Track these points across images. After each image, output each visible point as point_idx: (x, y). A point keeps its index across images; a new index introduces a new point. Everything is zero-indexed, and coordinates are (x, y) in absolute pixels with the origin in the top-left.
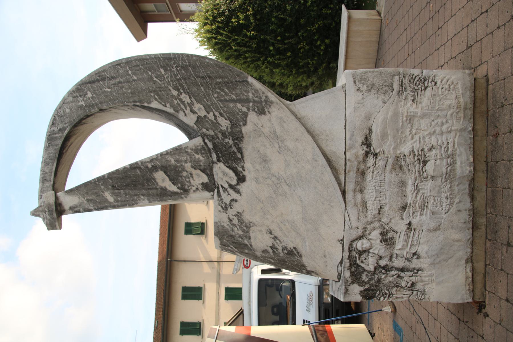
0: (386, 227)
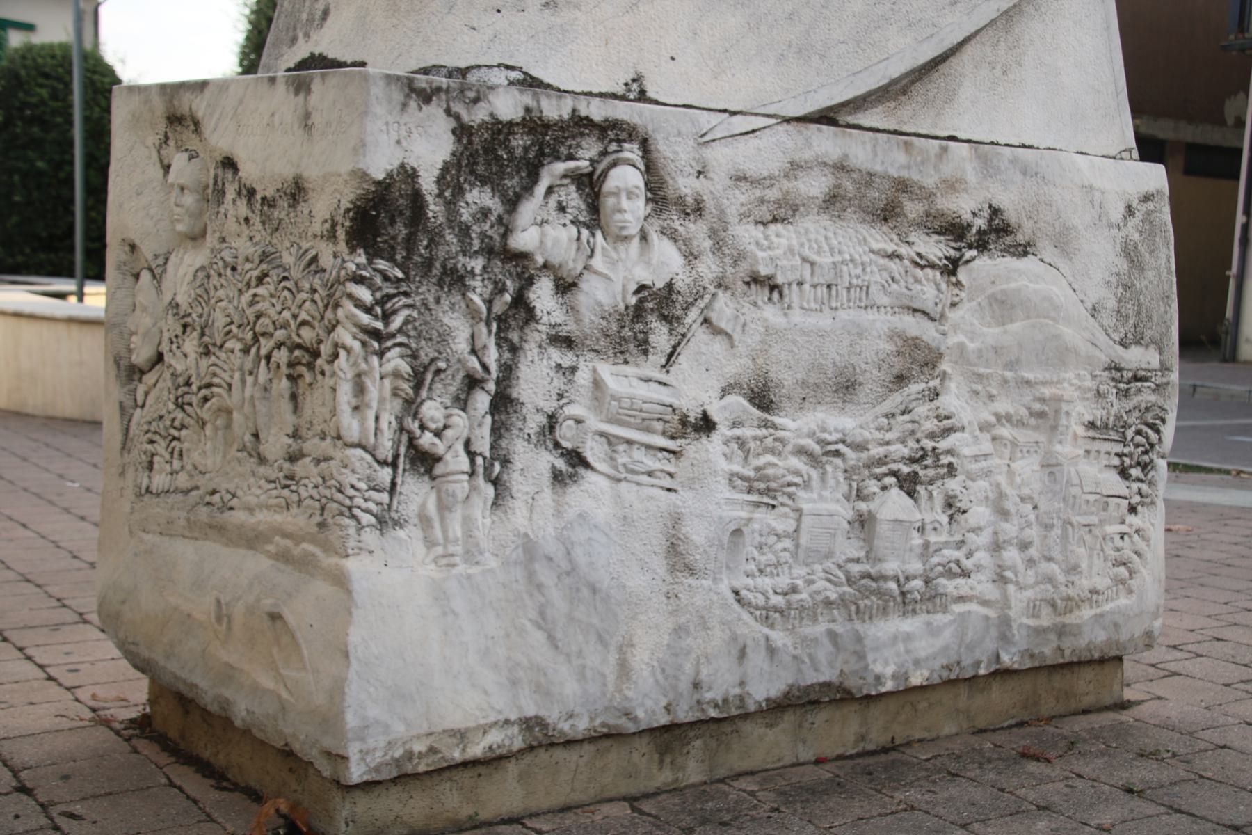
0: (693, 314)
